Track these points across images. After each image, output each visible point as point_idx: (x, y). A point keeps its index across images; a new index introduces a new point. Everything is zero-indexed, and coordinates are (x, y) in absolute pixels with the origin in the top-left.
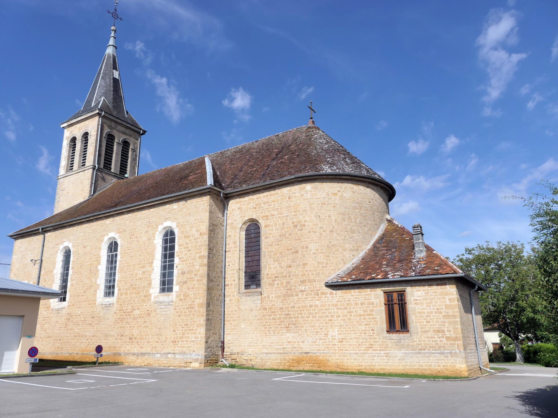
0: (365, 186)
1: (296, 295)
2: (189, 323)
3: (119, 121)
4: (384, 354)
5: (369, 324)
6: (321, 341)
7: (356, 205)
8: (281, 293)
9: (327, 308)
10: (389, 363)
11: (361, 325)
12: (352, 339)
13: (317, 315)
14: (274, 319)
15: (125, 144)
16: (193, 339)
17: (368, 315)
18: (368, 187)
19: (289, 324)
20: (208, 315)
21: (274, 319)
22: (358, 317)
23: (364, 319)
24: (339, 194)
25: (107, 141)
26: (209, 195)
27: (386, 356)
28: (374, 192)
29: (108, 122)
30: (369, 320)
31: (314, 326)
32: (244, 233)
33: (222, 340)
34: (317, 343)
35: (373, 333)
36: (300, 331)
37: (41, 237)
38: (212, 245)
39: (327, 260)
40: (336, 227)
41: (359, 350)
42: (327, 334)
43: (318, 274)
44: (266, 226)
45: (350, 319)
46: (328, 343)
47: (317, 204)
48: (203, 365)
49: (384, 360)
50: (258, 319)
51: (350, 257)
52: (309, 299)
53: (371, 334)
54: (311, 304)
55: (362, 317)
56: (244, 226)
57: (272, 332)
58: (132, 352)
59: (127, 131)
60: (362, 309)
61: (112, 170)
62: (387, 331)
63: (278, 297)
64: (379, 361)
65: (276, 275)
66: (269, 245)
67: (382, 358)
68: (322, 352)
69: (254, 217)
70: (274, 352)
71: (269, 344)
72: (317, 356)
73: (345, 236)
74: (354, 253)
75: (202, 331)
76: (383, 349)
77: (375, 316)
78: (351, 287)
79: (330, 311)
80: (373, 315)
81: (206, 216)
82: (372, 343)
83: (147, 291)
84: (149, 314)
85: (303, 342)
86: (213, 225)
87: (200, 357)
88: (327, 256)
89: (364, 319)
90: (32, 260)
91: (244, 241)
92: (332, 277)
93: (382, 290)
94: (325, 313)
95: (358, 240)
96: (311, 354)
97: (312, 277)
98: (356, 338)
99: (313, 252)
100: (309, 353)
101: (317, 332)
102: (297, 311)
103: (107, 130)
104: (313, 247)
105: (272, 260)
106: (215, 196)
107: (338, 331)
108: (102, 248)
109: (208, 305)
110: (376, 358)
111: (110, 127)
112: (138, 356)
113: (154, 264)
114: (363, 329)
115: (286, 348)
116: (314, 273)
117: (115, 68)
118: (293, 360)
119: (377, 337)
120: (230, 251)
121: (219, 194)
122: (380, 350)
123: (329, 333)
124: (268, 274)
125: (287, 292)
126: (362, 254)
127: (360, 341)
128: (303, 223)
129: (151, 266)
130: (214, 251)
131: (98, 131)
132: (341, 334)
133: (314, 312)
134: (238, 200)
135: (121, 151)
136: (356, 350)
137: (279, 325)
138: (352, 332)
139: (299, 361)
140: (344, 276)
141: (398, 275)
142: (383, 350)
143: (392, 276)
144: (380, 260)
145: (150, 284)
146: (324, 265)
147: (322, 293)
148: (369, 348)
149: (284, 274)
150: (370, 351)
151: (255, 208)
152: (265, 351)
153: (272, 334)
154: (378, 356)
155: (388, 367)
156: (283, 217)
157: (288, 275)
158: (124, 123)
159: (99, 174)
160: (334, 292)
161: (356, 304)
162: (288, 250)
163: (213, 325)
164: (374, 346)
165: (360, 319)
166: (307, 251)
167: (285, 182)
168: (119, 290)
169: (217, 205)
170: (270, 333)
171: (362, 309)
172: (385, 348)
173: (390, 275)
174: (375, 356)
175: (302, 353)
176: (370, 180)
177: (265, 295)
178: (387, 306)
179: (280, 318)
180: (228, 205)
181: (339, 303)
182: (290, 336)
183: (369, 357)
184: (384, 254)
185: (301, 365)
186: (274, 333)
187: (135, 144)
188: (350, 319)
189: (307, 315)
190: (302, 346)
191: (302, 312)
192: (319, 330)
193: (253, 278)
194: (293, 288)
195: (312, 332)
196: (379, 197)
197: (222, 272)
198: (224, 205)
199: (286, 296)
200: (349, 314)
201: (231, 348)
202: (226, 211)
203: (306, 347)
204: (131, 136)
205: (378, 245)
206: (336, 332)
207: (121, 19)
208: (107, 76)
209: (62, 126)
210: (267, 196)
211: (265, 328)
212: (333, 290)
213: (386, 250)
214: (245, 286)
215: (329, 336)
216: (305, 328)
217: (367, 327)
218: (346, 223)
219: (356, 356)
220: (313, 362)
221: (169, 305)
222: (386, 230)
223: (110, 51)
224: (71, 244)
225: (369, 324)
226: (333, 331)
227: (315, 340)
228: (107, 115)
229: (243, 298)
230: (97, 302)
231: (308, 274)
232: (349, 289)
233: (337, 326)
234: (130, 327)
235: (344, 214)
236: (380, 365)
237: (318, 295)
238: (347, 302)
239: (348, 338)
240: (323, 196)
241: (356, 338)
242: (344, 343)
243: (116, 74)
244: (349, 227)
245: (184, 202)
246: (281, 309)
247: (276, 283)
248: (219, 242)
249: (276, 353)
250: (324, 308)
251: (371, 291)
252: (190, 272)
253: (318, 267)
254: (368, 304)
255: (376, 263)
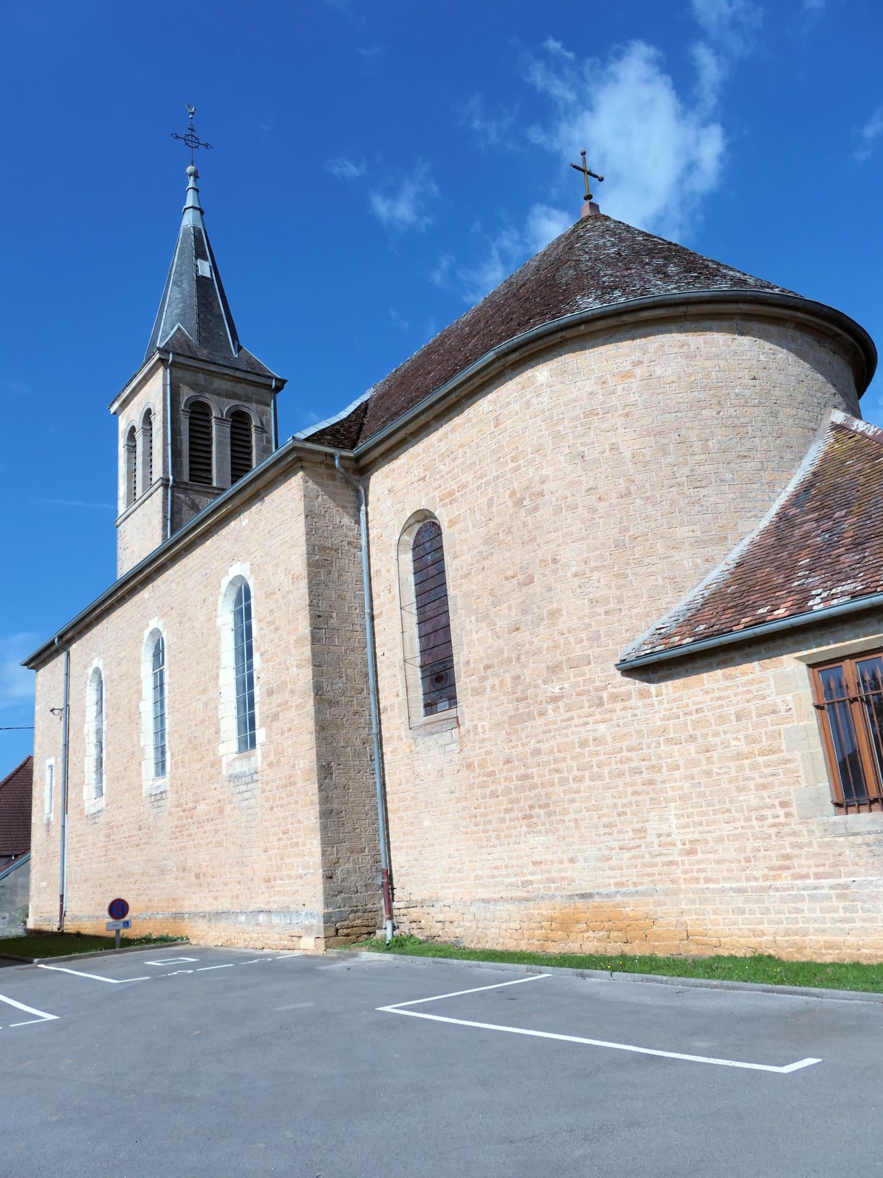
0: (730, 331)
1: (541, 714)
2: (290, 826)
3: (213, 368)
4: (832, 887)
5: (771, 785)
6: (626, 855)
7: (703, 396)
8: (503, 714)
9: (634, 742)
10: (853, 921)
11: (745, 789)
12: (720, 840)
13: (606, 770)
14: (494, 794)
15: (239, 421)
16: (300, 871)
17: (762, 753)
18: (741, 334)
19: (531, 807)
20: (325, 800)
21: (494, 794)
22: (732, 764)
23: (754, 767)
24: (639, 371)
25: (191, 418)
26: (302, 468)
27: (838, 897)
28: (767, 345)
29: (188, 376)
30: (767, 771)
31: (597, 808)
32: (408, 557)
33: (383, 865)
34: (613, 862)
35: (787, 815)
36: (561, 827)
37: (62, 657)
38: (323, 605)
39: (619, 587)
40: (638, 478)
41: (748, 879)
42: (643, 830)
43: (595, 638)
44: (452, 523)
45: (709, 773)
46: (647, 859)
47: (572, 419)
48: (322, 942)
49: (836, 910)
50: (459, 800)
51: (696, 566)
52: (576, 721)
53: (782, 819)
54: (584, 735)
55: (746, 762)
56: (406, 537)
57: (493, 835)
58: (200, 910)
59: (240, 388)
60: (741, 736)
61: (214, 484)
62: (838, 805)
63: (497, 726)
64: (818, 914)
65: (486, 662)
66: (462, 577)
67: (826, 904)
68: (632, 889)
69: (424, 505)
70: (504, 895)
71: (489, 872)
72: (617, 906)
73: (673, 503)
74: (710, 550)
75: (314, 846)
76: (826, 869)
77: (786, 755)
78: (699, 663)
79: (646, 751)
80: (780, 750)
81: (298, 529)
82: (789, 850)
83: (215, 752)
84: (221, 811)
85: (572, 861)
86: (323, 549)
87: (314, 922)
88: (618, 576)
89: (754, 767)
90: (52, 710)
91: (411, 579)
92: (638, 637)
93: (799, 658)
94: (630, 759)
95: (722, 507)
96: (597, 899)
97: (578, 651)
98: (735, 838)
99: (574, 569)
100: (590, 896)
101: (609, 825)
102: (548, 762)
103: (186, 394)
104: (570, 554)
105: (473, 618)
106: (323, 470)
107: (678, 817)
108: (143, 659)
109: (325, 771)
110: (805, 906)
111: (193, 386)
112: (210, 921)
113: (221, 681)
114: (754, 802)
115: (531, 882)
116: (584, 636)
117: (200, 254)
118: (552, 920)
119: (803, 828)
120: (381, 613)
121: (329, 461)
122: (817, 876)
123: (647, 825)
124: (468, 662)
125: (517, 709)
126: (738, 550)
127: (749, 846)
128: (538, 488)
129: (216, 685)
130: (334, 622)
131: (165, 399)
132: (687, 826)
133: (595, 760)
134: (386, 468)
135: (229, 435)
136: (738, 880)
137: (507, 811)
138: (719, 817)
139: (566, 924)
140: (674, 630)
141: (843, 594)
142: (828, 876)
143: (824, 600)
144: (790, 555)
145: (217, 732)
146: (612, 606)
147: (615, 698)
148: (780, 868)
149: (506, 655)
150: (785, 881)
151: (424, 479)
152: (483, 893)
153: (494, 841)
154: (813, 898)
155: (851, 939)
156: (488, 483)
157: (514, 656)
158: (226, 371)
159: (182, 496)
160: (653, 688)
161: (722, 719)
162: (507, 579)
163: (348, 827)
164: (796, 862)
165: (741, 768)
166: (555, 571)
167: (478, 381)
168: (173, 755)
169: (332, 496)
170: (489, 839)
171: (741, 736)
172: (834, 865)
173: (818, 600)
174: (802, 899)
175: (571, 897)
176: (745, 308)
177: (466, 725)
178: (826, 713)
179: (508, 791)
180: (366, 489)
181: (671, 723)
182: (536, 844)
183: (783, 901)
184: (807, 536)
185: (573, 936)
186: (498, 837)
187: (261, 415)
188: (709, 773)
189: (575, 772)
190: (569, 874)
191: (559, 766)
192: (614, 818)
193: (439, 681)
194: (530, 692)
195: (596, 827)
196: (792, 357)
197: (367, 675)
198: (357, 491)
199: (516, 719)
200: (702, 757)
201: (408, 889)
202: (363, 508)
203: (583, 878)
204: (249, 400)
205: (793, 511)
206: (673, 821)
207: (206, 145)
208: (184, 277)
209: (113, 410)
210: (446, 434)
211: (476, 825)
212: (650, 681)
213: (817, 520)
214: (426, 705)
215: (651, 837)
216: (572, 816)
217: (765, 793)
218: (670, 459)
219: (739, 901)
220: (607, 925)
221: (253, 782)
222: (827, 459)
223: (189, 220)
224: (101, 661)
225: (771, 785)
226: (662, 819)
227: (606, 852)
228: (181, 360)
229: (420, 741)
230: (144, 791)
231: (567, 643)
232: (696, 672)
233: (674, 800)
234: (195, 847)
235: (660, 433)
236: (823, 931)
237: (601, 704)
238: (695, 717)
239: (709, 837)
240: (589, 389)
241: (735, 838)
242: (700, 856)
243: (205, 268)
244: (686, 470)
245: (258, 505)
246: (508, 761)
247: (488, 684)
248: (349, 596)
249: (506, 900)
250: (625, 745)
251: (764, 668)
252: (282, 686)
253: (593, 615)
254: (759, 715)
255: (778, 568)
